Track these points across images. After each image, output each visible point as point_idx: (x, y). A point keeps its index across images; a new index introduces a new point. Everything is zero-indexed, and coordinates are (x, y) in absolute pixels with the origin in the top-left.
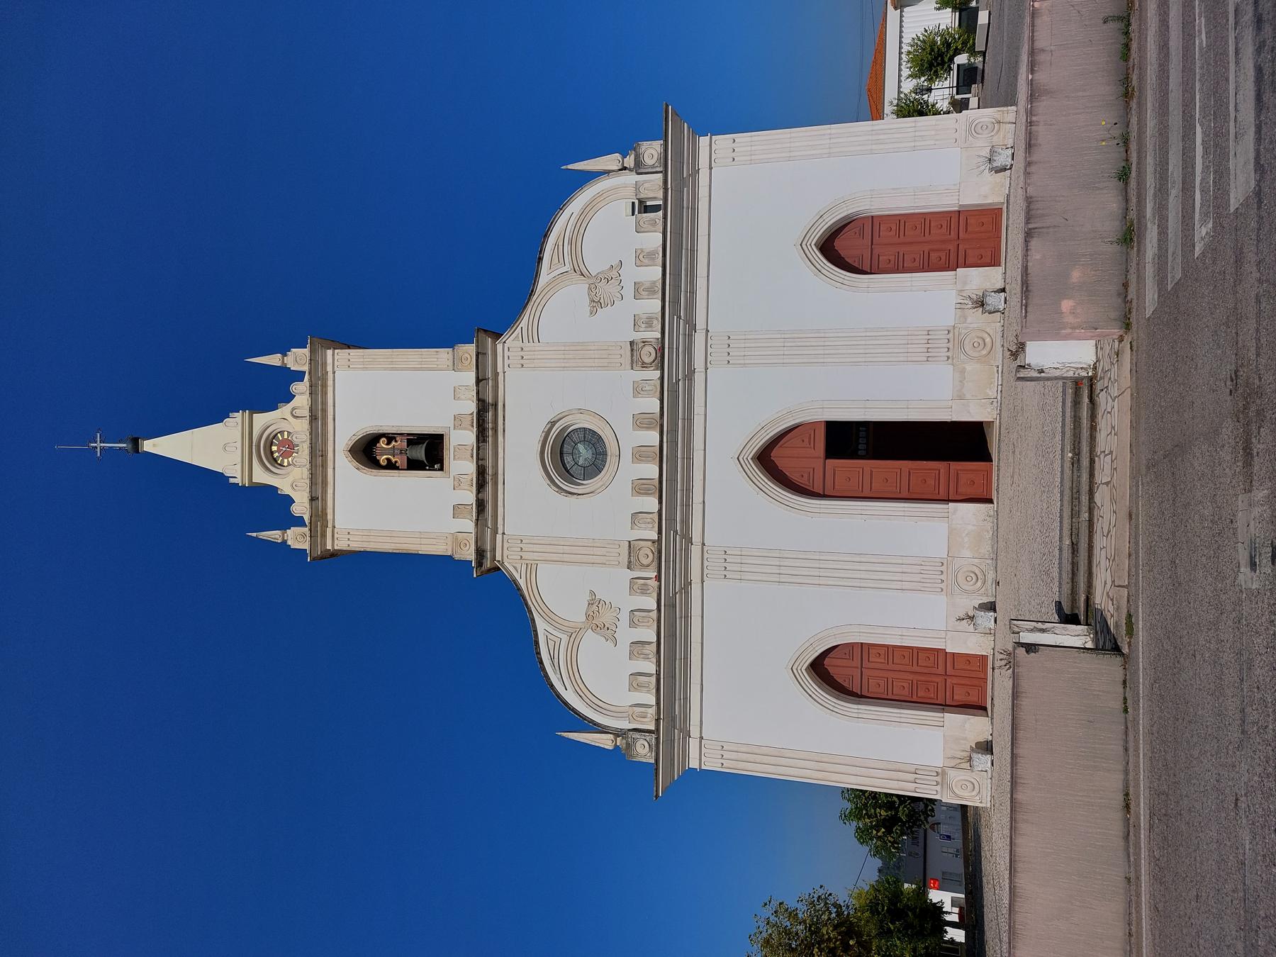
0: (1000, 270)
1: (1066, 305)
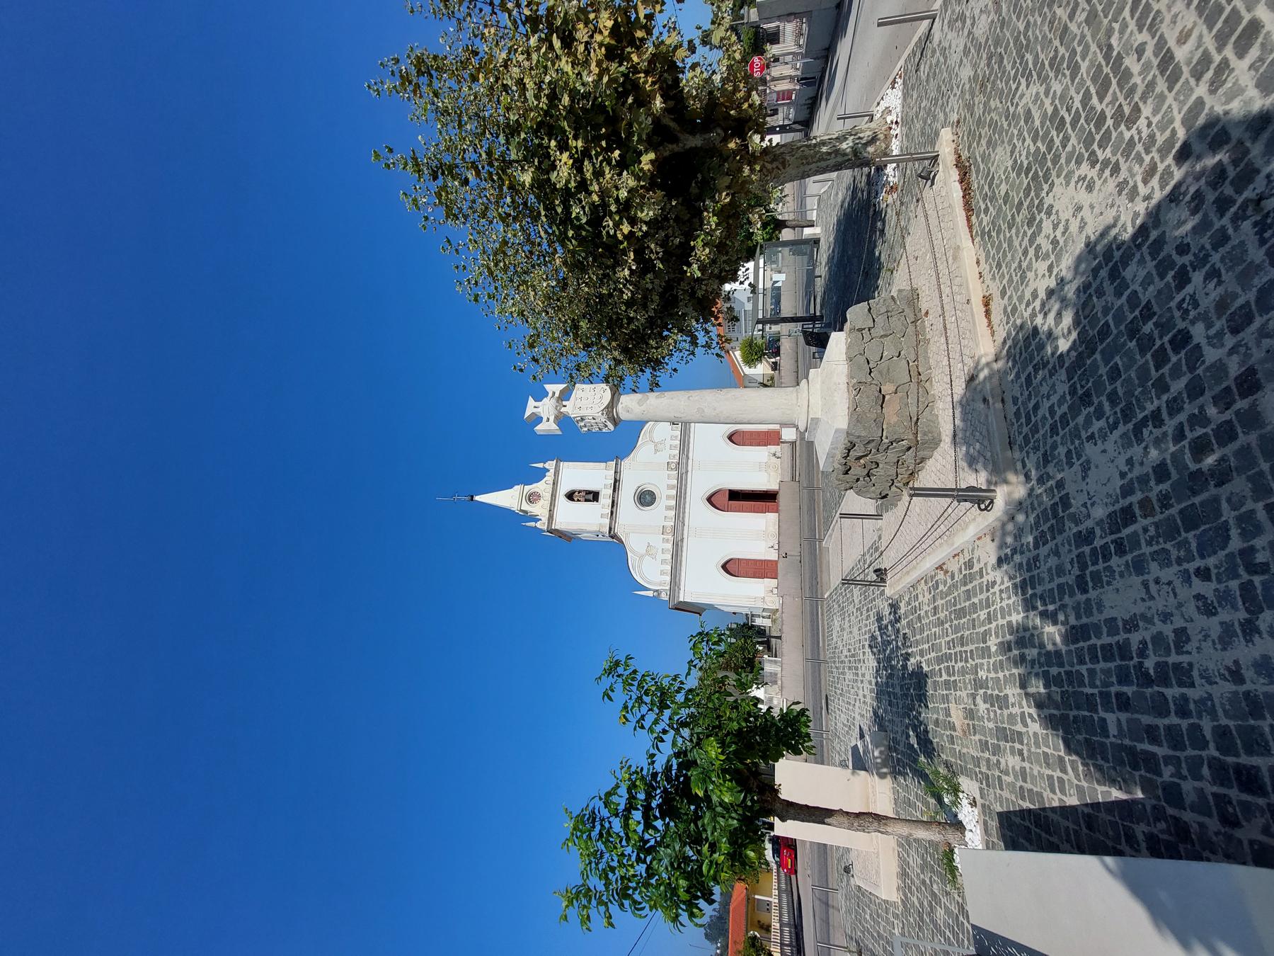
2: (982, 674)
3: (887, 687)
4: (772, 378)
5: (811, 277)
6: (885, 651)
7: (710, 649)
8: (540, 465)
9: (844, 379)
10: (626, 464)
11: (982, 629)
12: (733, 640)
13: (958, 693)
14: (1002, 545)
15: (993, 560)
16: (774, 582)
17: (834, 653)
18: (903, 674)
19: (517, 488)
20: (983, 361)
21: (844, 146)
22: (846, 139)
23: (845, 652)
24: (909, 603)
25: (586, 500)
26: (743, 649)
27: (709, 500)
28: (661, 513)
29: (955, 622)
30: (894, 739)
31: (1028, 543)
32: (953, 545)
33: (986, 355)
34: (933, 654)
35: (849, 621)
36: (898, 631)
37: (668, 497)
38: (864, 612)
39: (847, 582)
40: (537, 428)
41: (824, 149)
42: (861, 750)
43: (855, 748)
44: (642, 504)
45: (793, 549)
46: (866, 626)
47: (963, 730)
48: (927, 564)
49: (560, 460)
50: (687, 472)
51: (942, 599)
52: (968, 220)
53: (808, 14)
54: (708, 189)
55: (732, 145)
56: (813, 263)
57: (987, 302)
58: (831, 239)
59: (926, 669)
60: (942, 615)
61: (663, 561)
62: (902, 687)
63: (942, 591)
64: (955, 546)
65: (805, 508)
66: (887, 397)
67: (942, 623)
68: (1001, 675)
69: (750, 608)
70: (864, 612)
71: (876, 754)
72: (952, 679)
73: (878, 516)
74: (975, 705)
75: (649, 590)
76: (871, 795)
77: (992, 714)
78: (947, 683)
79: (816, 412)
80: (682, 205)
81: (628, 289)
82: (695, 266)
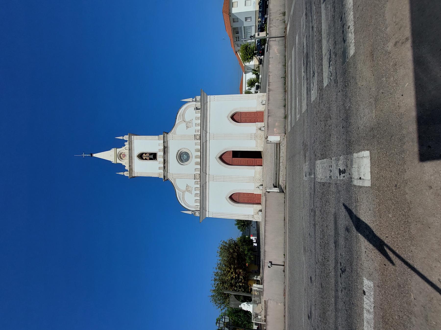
0: (264, 123)
1: (275, 129)
8: (121, 138)
10: (170, 136)
16: (259, 207)
19: (113, 150)
44: (182, 161)
50: (206, 141)
75: (189, 210)
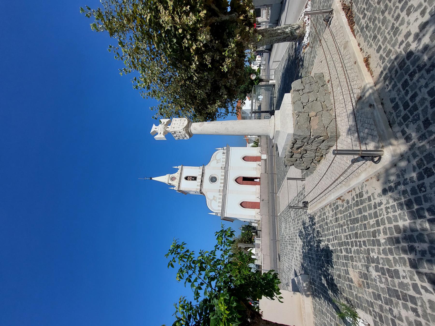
2: (374, 255)
3: (309, 254)
4: (258, 140)
5: (272, 99)
6: (307, 238)
7: (227, 239)
8: (176, 167)
9: (291, 112)
10: (206, 167)
11: (372, 230)
12: (244, 232)
13: (354, 263)
14: (387, 181)
15: (379, 190)
17: (282, 237)
18: (317, 250)
19: (167, 175)
20: (368, 86)
21: (287, 30)
22: (288, 28)
23: (287, 237)
24: (320, 217)
25: (192, 180)
26: (248, 234)
27: (236, 180)
28: (219, 185)
29: (350, 225)
30: (313, 279)
31: (412, 177)
32: (350, 185)
33: (369, 83)
34: (336, 242)
35: (289, 225)
36: (314, 229)
37: (221, 179)
38: (296, 221)
39: (290, 207)
40: (155, 137)
41: (279, 31)
42: (296, 282)
43: (293, 280)
44: (212, 182)
45: (265, 197)
46: (297, 227)
47: (359, 284)
48: (332, 197)
49: (183, 165)
50: (228, 171)
51: (341, 214)
52: (352, 28)
53: (271, 5)
54: (231, 35)
55: (241, 18)
56: (272, 94)
57: (367, 61)
58: (280, 82)
59: (331, 248)
60: (341, 222)
61: (219, 202)
62: (316, 255)
63: (341, 210)
64: (351, 186)
65: (270, 183)
66: (312, 118)
67: (342, 226)
68: (390, 257)
69: (250, 219)
70: (296, 221)
71: (304, 285)
72: (350, 255)
73: (303, 179)
74: (368, 271)
75: (214, 212)
76: (302, 304)
77: (383, 280)
78: (346, 257)
79: (278, 128)
80: (220, 43)
81: (196, 76)
82: (225, 66)
